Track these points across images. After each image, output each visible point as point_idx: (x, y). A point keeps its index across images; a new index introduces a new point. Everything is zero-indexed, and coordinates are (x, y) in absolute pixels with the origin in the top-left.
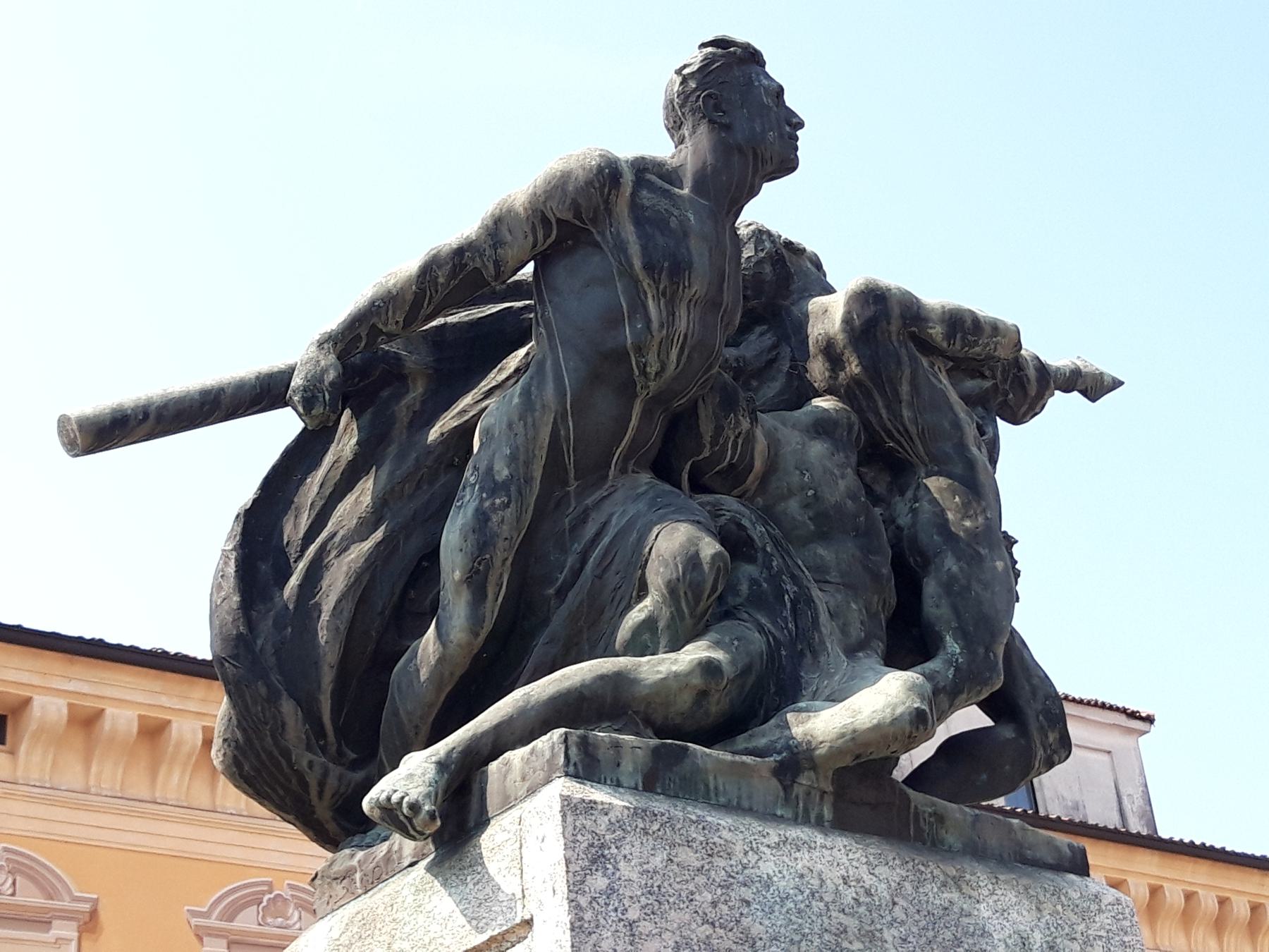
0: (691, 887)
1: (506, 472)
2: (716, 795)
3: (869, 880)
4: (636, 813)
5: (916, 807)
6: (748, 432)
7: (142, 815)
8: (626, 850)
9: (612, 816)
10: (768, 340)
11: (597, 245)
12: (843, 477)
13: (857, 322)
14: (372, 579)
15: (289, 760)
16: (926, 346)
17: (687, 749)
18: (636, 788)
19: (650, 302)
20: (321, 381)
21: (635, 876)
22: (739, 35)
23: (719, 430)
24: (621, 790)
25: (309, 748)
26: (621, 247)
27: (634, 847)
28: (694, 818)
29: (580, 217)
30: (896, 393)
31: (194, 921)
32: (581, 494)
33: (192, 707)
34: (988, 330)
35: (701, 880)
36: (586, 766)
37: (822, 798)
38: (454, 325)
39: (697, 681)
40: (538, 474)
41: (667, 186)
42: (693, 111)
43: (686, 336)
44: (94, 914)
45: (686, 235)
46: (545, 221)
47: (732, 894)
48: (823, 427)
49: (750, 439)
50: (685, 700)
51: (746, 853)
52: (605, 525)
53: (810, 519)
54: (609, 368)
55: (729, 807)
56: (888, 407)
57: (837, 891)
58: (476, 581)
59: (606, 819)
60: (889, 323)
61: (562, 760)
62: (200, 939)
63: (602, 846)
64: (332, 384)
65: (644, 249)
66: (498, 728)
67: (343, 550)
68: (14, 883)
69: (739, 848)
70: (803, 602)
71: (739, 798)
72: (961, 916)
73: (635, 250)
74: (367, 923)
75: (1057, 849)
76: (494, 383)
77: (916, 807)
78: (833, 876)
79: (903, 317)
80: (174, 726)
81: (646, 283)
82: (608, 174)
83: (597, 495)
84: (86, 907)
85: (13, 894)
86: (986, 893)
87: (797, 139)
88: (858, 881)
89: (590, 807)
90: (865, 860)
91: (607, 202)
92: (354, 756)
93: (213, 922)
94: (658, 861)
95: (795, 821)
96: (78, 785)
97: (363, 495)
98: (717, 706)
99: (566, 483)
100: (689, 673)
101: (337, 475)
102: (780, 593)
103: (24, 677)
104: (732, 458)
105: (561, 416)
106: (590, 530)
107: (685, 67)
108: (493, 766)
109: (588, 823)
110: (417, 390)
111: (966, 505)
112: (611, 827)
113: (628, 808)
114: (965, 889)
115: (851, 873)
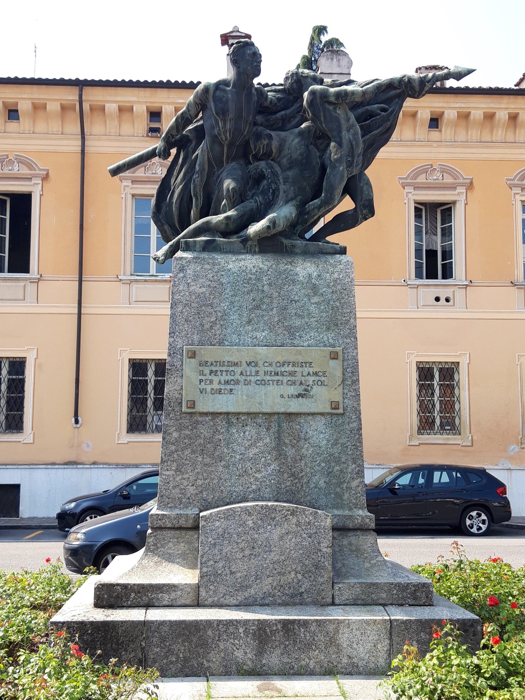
0: (207, 273)
3: (261, 266)
6: (267, 144)
7: (488, 147)
9: (187, 260)
14: (183, 194)
21: (191, 273)
27: (192, 266)
31: (508, 182)
32: (218, 170)
33: (503, 106)
34: (350, 94)
35: (210, 272)
39: (224, 222)
44: (471, 183)
45: (227, 101)
49: (269, 145)
50: (223, 226)
57: (251, 270)
62: (511, 189)
68: (443, 175)
73: (213, 110)
75: (335, 248)
78: (250, 266)
79: (321, 97)
80: (497, 114)
81: (217, 117)
83: (222, 170)
84: (469, 181)
85: (443, 179)
91: (207, 97)
93: (516, 182)
95: (247, 253)
96: (463, 140)
98: (232, 227)
100: (223, 220)
103: (441, 105)
112: (187, 262)
114: (293, 264)
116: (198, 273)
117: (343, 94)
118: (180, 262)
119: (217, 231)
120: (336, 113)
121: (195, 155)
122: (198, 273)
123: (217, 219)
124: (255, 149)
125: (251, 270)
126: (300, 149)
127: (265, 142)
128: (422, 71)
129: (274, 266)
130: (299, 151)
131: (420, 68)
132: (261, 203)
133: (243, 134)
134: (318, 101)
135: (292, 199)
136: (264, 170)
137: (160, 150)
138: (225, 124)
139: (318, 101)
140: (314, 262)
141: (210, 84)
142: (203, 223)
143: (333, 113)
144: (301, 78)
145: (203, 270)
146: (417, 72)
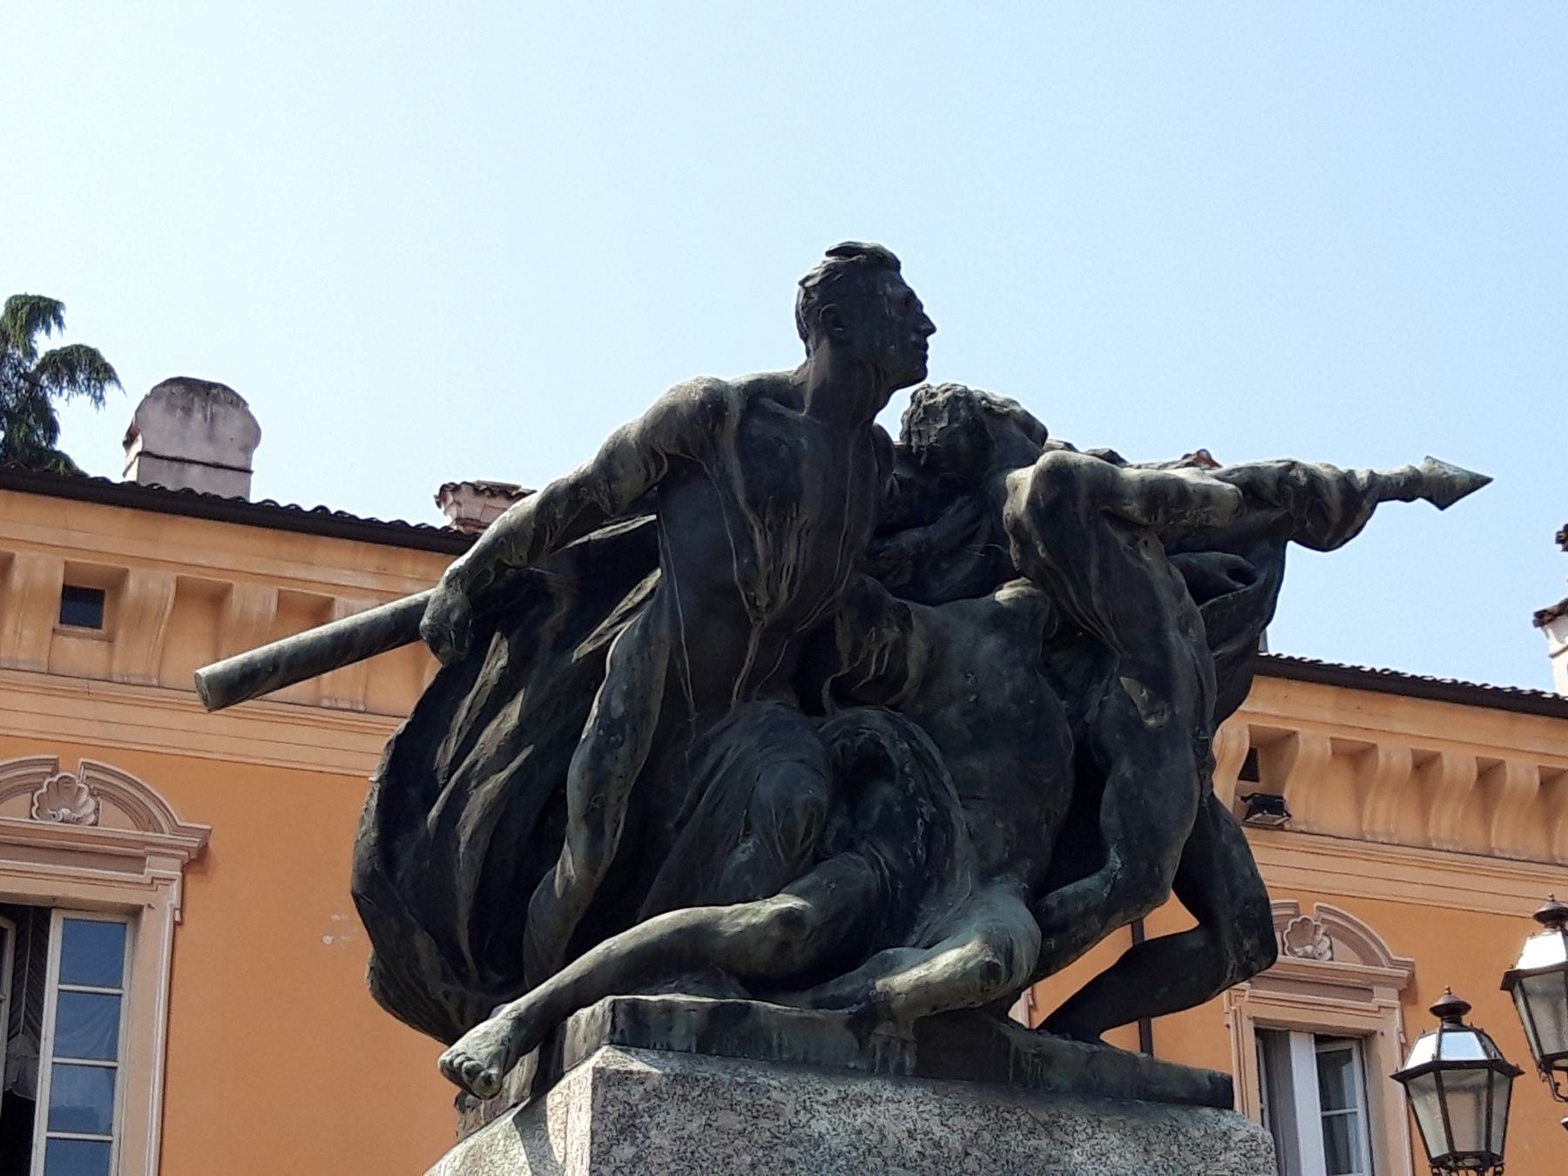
0: (729, 1151)
1: (621, 709)
2: (780, 1051)
3: (938, 1132)
4: (677, 1079)
5: (1017, 1050)
6: (896, 643)
8: (659, 1119)
10: (967, 514)
11: (706, 476)
12: (1011, 677)
13: (1042, 504)
15: (425, 990)
16: (1124, 522)
17: (749, 1007)
18: (689, 1051)
19: (757, 536)
20: (447, 619)
21: (666, 1143)
22: (867, 240)
23: (857, 646)
24: (670, 1055)
25: (445, 978)
26: (726, 480)
27: (670, 1115)
28: (742, 1080)
29: (692, 447)
30: (1085, 578)
34: (1197, 499)
35: (740, 1143)
36: (632, 1031)
37: (903, 1047)
38: (598, 541)
39: (775, 933)
40: (656, 708)
41: (782, 409)
42: (817, 325)
43: (795, 568)
46: (655, 454)
47: (775, 1155)
48: (1001, 618)
49: (900, 648)
50: (765, 952)
51: (797, 1113)
52: (723, 756)
53: (969, 727)
54: (716, 600)
55: (799, 1063)
56: (1077, 592)
57: (899, 1146)
58: (594, 817)
59: (641, 1089)
60: (1075, 505)
61: (608, 1027)
63: (634, 1115)
64: (457, 624)
65: (748, 485)
66: (578, 982)
67: (483, 780)
69: (788, 1110)
70: (941, 824)
71: (806, 1053)
72: (1048, 1162)
73: (739, 484)
74: (474, 1158)
76: (630, 605)
77: (1017, 1050)
79: (1092, 496)
81: (751, 518)
82: (712, 406)
83: (723, 723)
86: (1084, 1136)
87: (926, 347)
88: (926, 1134)
89: (625, 1077)
90: (937, 1111)
91: (712, 437)
92: (500, 979)
94: (693, 1127)
95: (870, 1073)
97: (512, 714)
98: (800, 956)
99: (687, 715)
101: (482, 700)
102: (912, 815)
104: (877, 670)
105: (676, 651)
106: (709, 761)
107: (808, 278)
108: (570, 1020)
109: (620, 1094)
110: (562, 610)
111: (1152, 701)
112: (646, 1096)
113: (667, 1076)
114: (1058, 1134)
115: (919, 1126)
116: (692, 1145)
117: (1173, 495)
118: (620, 1094)
119: (731, 972)
120: (1141, 560)
121: (586, 647)
122: (692, 1145)
123: (742, 921)
124: (853, 657)
125: (899, 1146)
126: (1011, 677)
127: (892, 634)
128: (459, 498)
129: (986, 1136)
130: (1008, 686)
131: (455, 488)
132: (891, 873)
133: (832, 592)
134: (1082, 506)
135: (1002, 868)
136: (884, 742)
137: (442, 617)
138: (779, 546)
139: (1082, 506)
140: (1134, 1130)
141: (727, 387)
142: (680, 931)
143: (1130, 560)
144: (986, 418)
145: (713, 1133)
146: (441, 499)
